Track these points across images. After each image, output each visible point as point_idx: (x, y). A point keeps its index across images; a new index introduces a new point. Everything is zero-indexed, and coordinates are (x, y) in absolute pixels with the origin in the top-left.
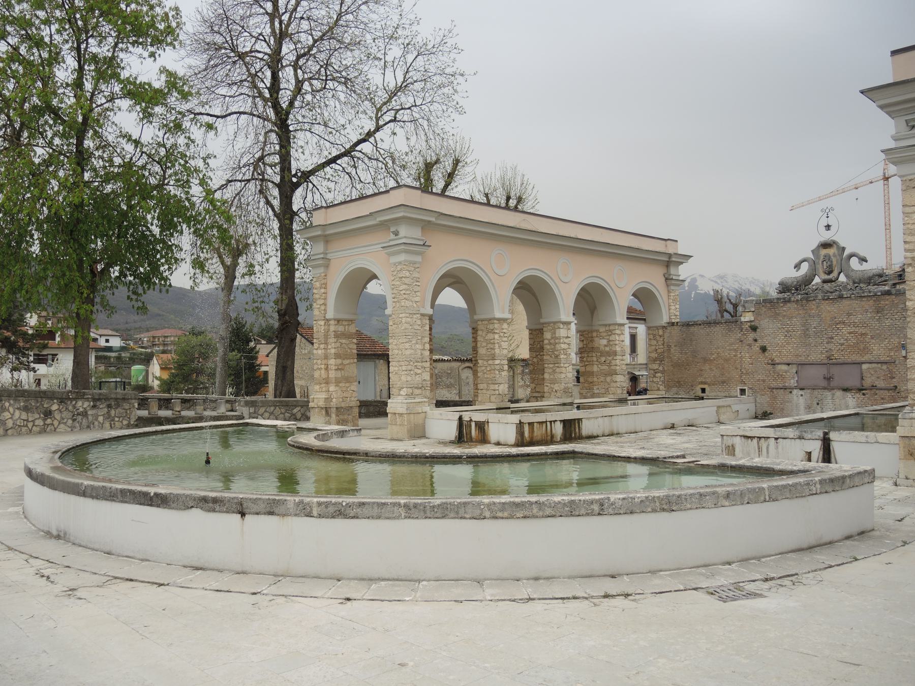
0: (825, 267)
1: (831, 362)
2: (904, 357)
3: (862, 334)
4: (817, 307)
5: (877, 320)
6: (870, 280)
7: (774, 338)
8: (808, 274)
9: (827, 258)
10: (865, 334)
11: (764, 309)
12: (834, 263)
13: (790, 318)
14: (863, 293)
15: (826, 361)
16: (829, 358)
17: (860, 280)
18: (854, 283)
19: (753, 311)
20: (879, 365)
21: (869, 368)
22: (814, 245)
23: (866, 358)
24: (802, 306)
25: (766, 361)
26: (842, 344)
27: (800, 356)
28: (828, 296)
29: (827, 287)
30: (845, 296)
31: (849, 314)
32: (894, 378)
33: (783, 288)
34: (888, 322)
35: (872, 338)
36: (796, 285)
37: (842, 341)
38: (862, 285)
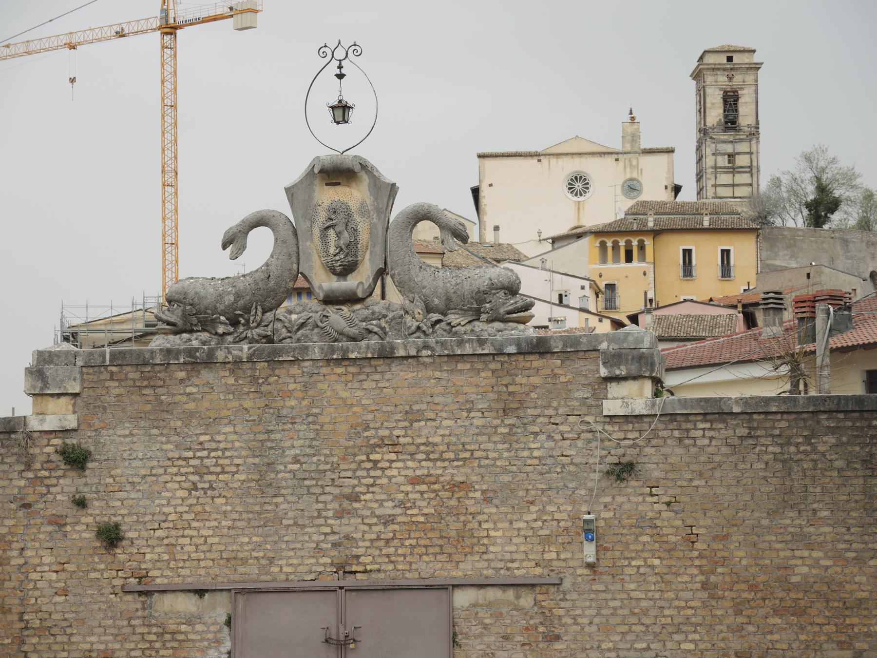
0: (332, 250)
1: (349, 581)
2: (590, 566)
3: (455, 487)
4: (306, 387)
5: (505, 440)
6: (481, 302)
7: (151, 497)
8: (274, 270)
9: (339, 219)
10: (464, 486)
11: (116, 389)
12: (364, 237)
13: (212, 423)
14: (461, 343)
15: (331, 581)
16: (343, 569)
17: (449, 300)
18: (429, 309)
19: (75, 395)
20: (510, 594)
21: (475, 605)
22: (296, 172)
23: (468, 568)
24: (254, 380)
25: (118, 582)
26: (388, 520)
27: (244, 561)
28: (346, 351)
29: (338, 317)
30: (401, 353)
31: (412, 417)
32: (558, 638)
33: (185, 316)
34: (538, 447)
35: (487, 500)
36: (232, 306)
37: (388, 509)
38: (453, 318)
